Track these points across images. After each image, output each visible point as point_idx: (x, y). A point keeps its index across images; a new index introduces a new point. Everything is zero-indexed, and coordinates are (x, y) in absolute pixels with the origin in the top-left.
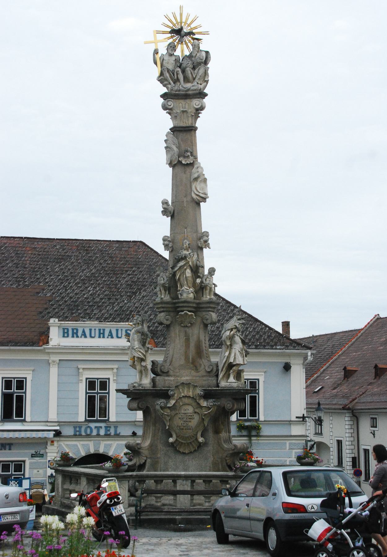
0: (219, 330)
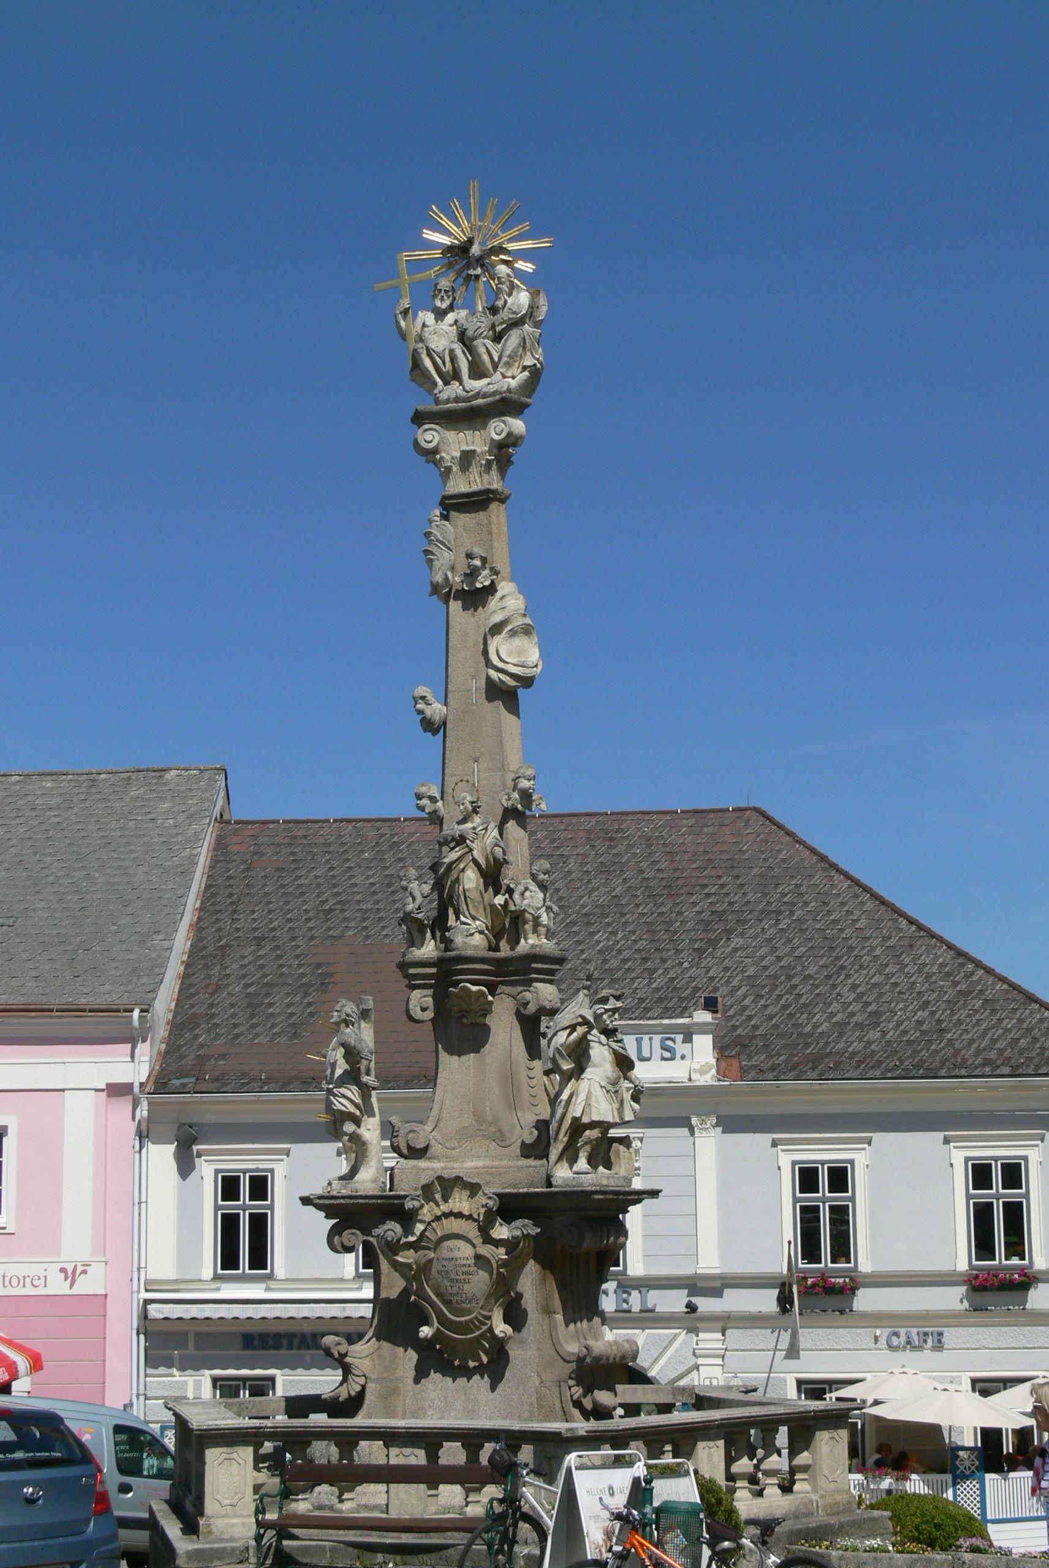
0: (922, 1029)
